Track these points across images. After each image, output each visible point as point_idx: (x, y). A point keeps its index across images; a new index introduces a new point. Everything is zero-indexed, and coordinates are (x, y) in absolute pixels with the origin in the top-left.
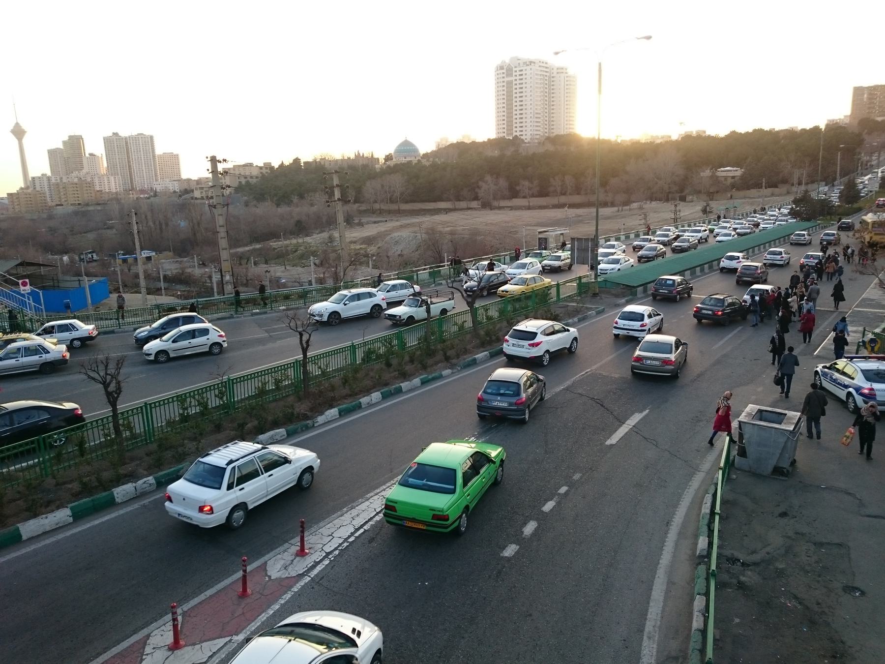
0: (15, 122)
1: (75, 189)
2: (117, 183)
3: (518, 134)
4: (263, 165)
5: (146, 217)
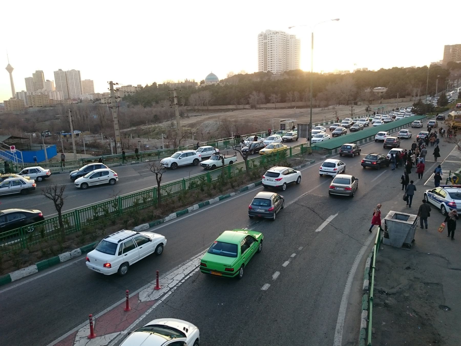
0: (8, 64)
1: (39, 98)
2: (61, 96)
3: (270, 70)
4: (137, 86)
5: (76, 113)
